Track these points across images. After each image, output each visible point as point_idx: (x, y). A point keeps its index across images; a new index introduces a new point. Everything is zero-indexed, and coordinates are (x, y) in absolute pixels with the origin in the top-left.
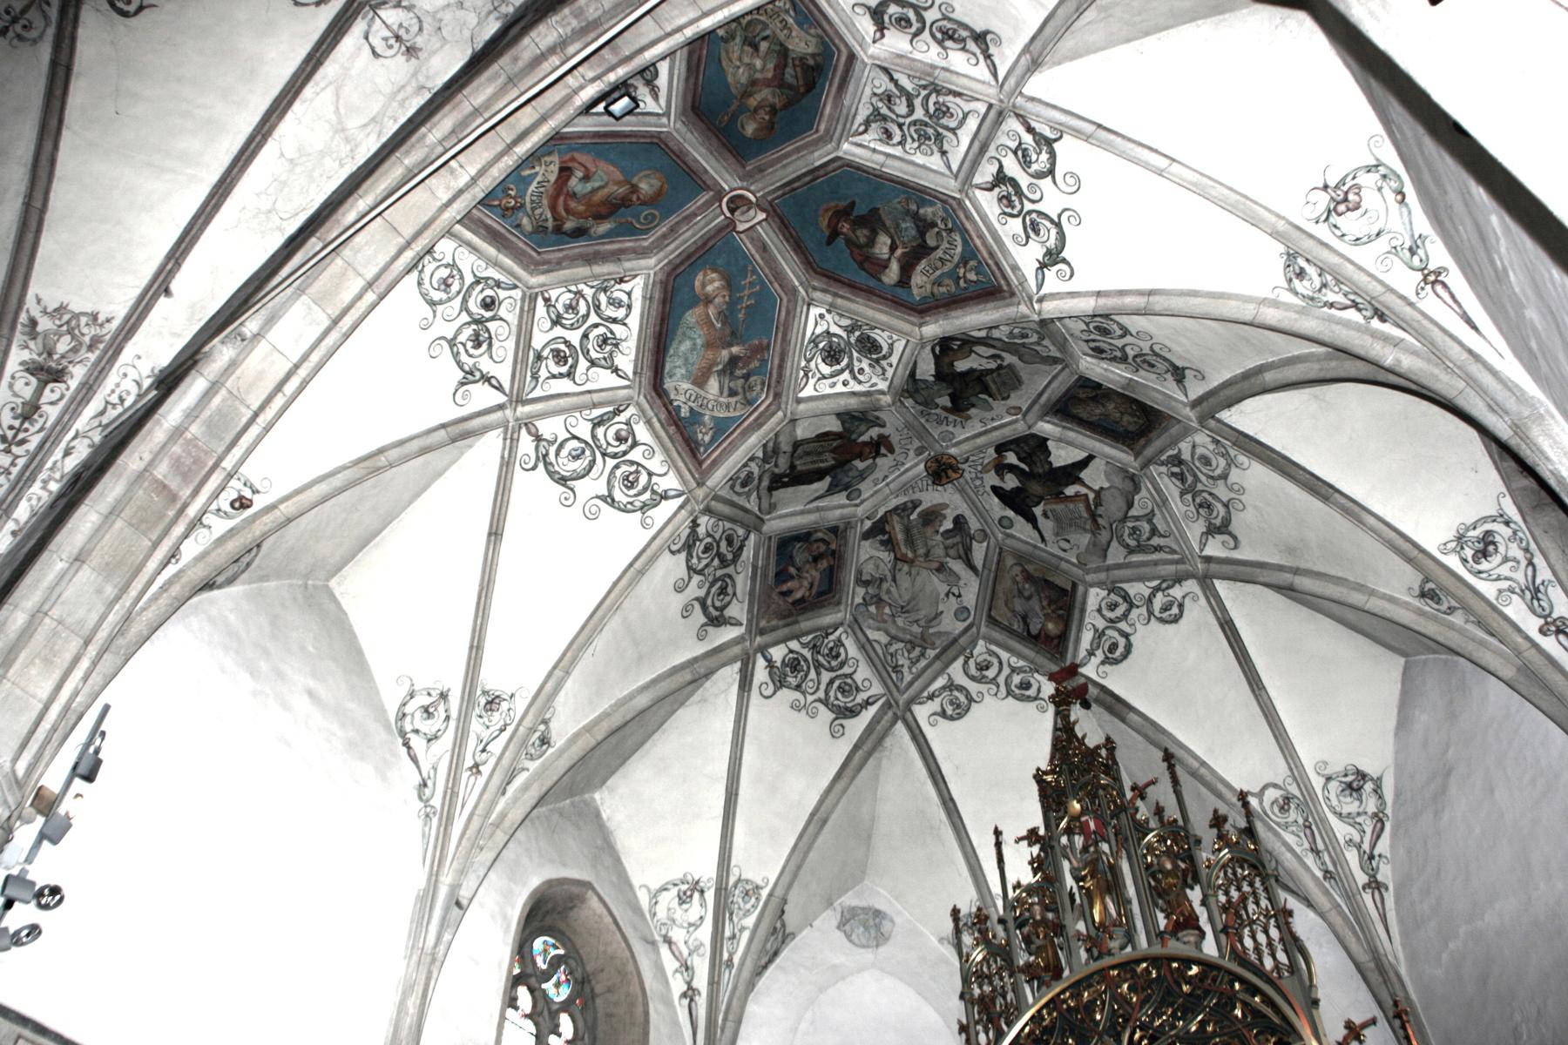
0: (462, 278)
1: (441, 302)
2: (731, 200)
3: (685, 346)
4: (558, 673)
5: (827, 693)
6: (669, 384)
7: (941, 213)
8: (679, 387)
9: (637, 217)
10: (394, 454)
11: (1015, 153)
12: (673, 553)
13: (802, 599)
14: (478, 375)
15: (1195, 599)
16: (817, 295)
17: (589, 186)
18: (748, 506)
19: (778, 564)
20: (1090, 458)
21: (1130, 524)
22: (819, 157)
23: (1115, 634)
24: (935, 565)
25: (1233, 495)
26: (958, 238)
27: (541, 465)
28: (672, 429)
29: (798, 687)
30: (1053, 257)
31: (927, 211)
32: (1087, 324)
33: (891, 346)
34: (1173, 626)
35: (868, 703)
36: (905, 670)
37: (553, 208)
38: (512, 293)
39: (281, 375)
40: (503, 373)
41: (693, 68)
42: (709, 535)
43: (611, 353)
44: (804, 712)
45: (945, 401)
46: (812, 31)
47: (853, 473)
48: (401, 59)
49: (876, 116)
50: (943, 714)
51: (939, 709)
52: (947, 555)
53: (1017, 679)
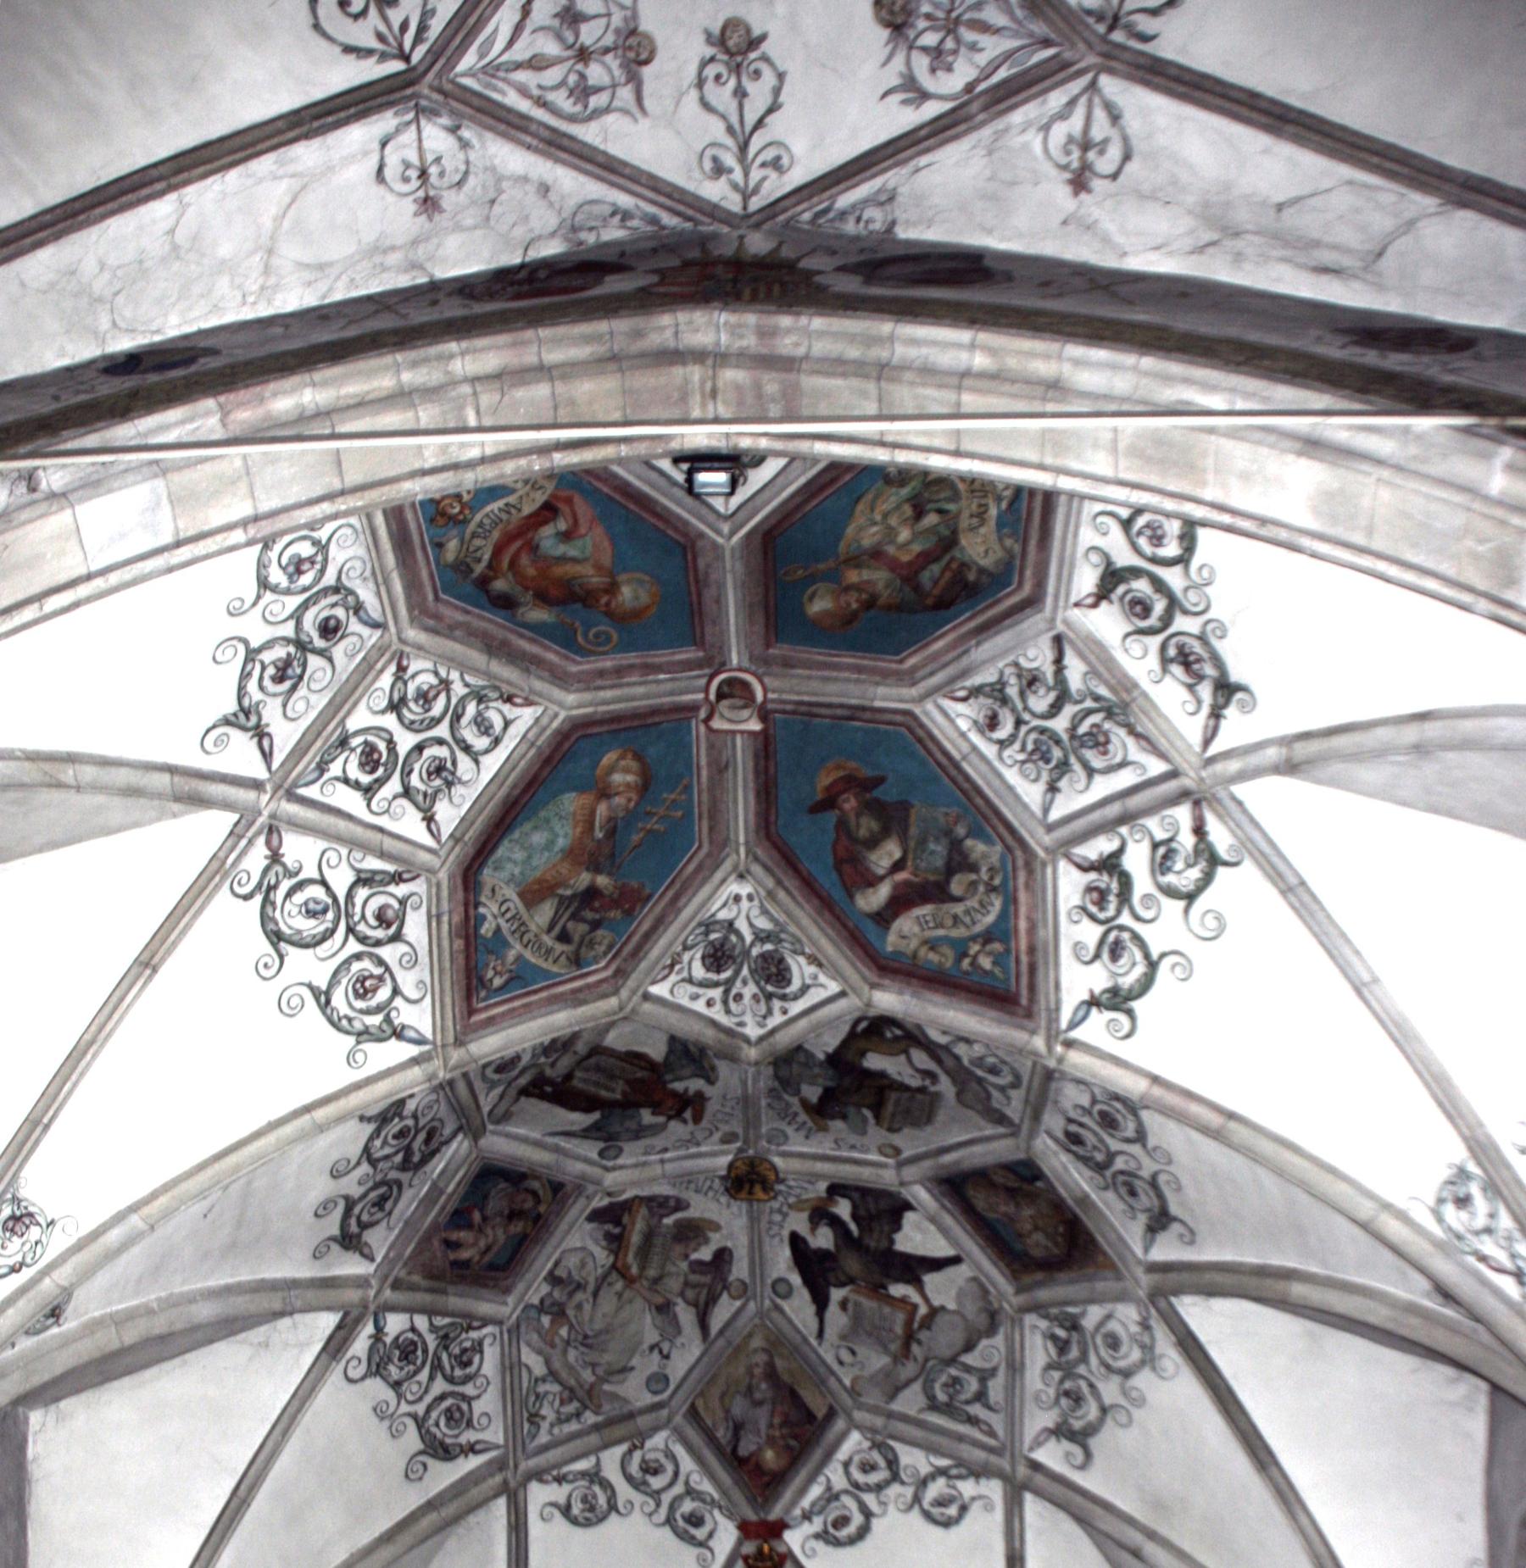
0: (322, 571)
1: (275, 589)
2: (730, 682)
3: (538, 838)
4: (135, 1220)
9: (588, 627)
10: (89, 773)
11: (1155, 846)
13: (466, 1264)
14: (254, 719)
15: (989, 1507)
16: (757, 869)
17: (561, 549)
18: (481, 1099)
20: (955, 1260)
21: (953, 1372)
22: (886, 697)
24: (659, 1300)
25: (1123, 1402)
26: (997, 903)
27: (259, 898)
28: (459, 944)
29: (396, 1385)
30: (1117, 1000)
31: (977, 848)
32: (1094, 1101)
33: (804, 989)
35: (471, 1449)
36: (545, 1426)
37: (498, 551)
38: (365, 631)
39: (63, 578)
40: (285, 736)
41: (812, 489)
43: (437, 791)
44: (386, 1423)
45: (813, 1093)
46: (1008, 542)
47: (631, 1124)
48: (409, 206)
49: (997, 691)
50: (566, 1511)
51: (562, 1501)
52: (682, 1294)
53: (688, 1506)
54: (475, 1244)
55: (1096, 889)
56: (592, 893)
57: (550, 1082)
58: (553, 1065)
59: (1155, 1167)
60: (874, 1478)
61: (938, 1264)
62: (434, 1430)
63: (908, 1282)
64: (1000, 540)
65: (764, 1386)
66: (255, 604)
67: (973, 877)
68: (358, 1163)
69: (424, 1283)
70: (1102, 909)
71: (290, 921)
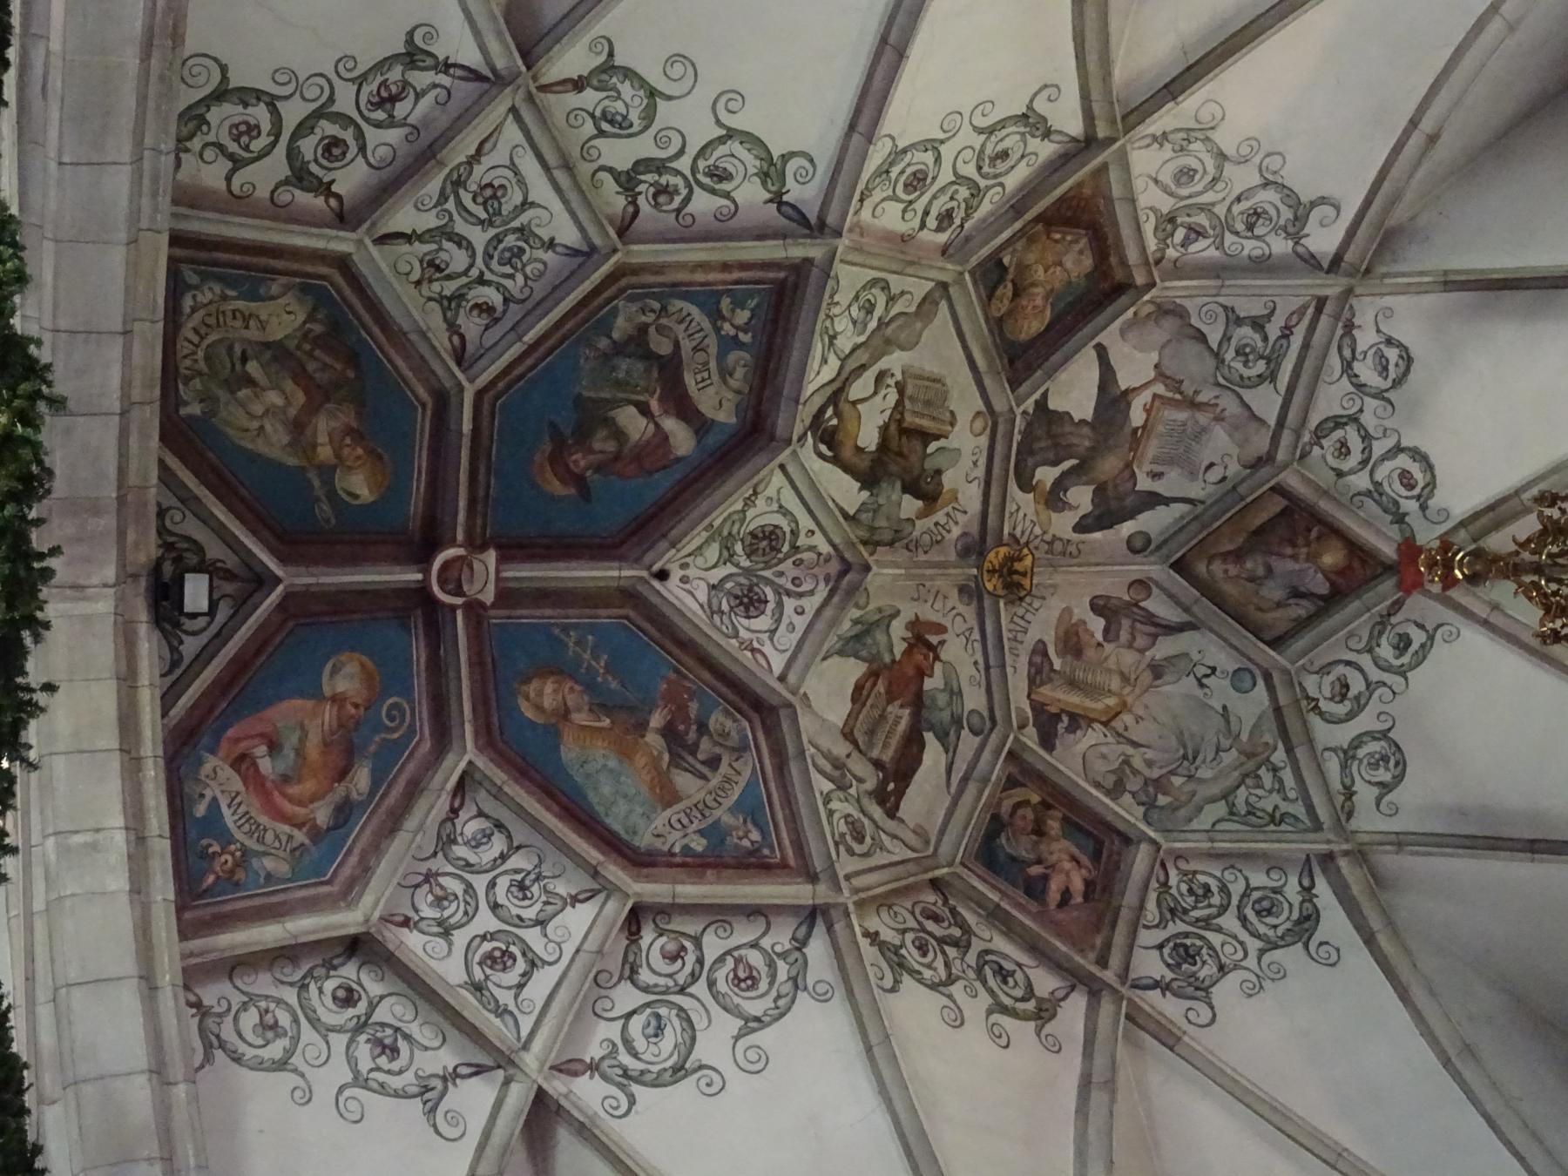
1: (289, 1053)
3: (606, 789)
5: (1255, 935)
6: (644, 841)
7: (634, 308)
8: (656, 829)
9: (379, 727)
11: (602, 133)
12: (893, 990)
13: (1089, 884)
18: (895, 858)
19: (1014, 884)
23: (1388, 466)
24: (1147, 677)
26: (678, 304)
31: (621, 327)
32: (894, 198)
34: (1415, 367)
36: (1285, 807)
42: (904, 931)
44: (1267, 984)
45: (910, 505)
46: (275, 289)
47: (942, 699)
50: (1385, 787)
52: (1142, 651)
53: (1386, 651)
54: (1067, 874)
55: (655, 196)
56: (668, 732)
57: (883, 784)
58: (860, 780)
59: (967, 128)
60: (1355, 443)
61: (1107, 373)
62: (1280, 931)
63: (1129, 405)
64: (273, 298)
65: (1249, 565)
66: (302, 1075)
67: (652, 330)
68: (950, 997)
69: (1105, 931)
70: (677, 192)
71: (664, 1055)
